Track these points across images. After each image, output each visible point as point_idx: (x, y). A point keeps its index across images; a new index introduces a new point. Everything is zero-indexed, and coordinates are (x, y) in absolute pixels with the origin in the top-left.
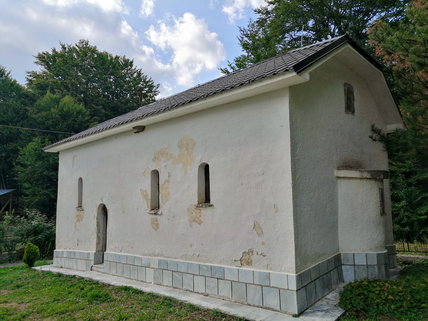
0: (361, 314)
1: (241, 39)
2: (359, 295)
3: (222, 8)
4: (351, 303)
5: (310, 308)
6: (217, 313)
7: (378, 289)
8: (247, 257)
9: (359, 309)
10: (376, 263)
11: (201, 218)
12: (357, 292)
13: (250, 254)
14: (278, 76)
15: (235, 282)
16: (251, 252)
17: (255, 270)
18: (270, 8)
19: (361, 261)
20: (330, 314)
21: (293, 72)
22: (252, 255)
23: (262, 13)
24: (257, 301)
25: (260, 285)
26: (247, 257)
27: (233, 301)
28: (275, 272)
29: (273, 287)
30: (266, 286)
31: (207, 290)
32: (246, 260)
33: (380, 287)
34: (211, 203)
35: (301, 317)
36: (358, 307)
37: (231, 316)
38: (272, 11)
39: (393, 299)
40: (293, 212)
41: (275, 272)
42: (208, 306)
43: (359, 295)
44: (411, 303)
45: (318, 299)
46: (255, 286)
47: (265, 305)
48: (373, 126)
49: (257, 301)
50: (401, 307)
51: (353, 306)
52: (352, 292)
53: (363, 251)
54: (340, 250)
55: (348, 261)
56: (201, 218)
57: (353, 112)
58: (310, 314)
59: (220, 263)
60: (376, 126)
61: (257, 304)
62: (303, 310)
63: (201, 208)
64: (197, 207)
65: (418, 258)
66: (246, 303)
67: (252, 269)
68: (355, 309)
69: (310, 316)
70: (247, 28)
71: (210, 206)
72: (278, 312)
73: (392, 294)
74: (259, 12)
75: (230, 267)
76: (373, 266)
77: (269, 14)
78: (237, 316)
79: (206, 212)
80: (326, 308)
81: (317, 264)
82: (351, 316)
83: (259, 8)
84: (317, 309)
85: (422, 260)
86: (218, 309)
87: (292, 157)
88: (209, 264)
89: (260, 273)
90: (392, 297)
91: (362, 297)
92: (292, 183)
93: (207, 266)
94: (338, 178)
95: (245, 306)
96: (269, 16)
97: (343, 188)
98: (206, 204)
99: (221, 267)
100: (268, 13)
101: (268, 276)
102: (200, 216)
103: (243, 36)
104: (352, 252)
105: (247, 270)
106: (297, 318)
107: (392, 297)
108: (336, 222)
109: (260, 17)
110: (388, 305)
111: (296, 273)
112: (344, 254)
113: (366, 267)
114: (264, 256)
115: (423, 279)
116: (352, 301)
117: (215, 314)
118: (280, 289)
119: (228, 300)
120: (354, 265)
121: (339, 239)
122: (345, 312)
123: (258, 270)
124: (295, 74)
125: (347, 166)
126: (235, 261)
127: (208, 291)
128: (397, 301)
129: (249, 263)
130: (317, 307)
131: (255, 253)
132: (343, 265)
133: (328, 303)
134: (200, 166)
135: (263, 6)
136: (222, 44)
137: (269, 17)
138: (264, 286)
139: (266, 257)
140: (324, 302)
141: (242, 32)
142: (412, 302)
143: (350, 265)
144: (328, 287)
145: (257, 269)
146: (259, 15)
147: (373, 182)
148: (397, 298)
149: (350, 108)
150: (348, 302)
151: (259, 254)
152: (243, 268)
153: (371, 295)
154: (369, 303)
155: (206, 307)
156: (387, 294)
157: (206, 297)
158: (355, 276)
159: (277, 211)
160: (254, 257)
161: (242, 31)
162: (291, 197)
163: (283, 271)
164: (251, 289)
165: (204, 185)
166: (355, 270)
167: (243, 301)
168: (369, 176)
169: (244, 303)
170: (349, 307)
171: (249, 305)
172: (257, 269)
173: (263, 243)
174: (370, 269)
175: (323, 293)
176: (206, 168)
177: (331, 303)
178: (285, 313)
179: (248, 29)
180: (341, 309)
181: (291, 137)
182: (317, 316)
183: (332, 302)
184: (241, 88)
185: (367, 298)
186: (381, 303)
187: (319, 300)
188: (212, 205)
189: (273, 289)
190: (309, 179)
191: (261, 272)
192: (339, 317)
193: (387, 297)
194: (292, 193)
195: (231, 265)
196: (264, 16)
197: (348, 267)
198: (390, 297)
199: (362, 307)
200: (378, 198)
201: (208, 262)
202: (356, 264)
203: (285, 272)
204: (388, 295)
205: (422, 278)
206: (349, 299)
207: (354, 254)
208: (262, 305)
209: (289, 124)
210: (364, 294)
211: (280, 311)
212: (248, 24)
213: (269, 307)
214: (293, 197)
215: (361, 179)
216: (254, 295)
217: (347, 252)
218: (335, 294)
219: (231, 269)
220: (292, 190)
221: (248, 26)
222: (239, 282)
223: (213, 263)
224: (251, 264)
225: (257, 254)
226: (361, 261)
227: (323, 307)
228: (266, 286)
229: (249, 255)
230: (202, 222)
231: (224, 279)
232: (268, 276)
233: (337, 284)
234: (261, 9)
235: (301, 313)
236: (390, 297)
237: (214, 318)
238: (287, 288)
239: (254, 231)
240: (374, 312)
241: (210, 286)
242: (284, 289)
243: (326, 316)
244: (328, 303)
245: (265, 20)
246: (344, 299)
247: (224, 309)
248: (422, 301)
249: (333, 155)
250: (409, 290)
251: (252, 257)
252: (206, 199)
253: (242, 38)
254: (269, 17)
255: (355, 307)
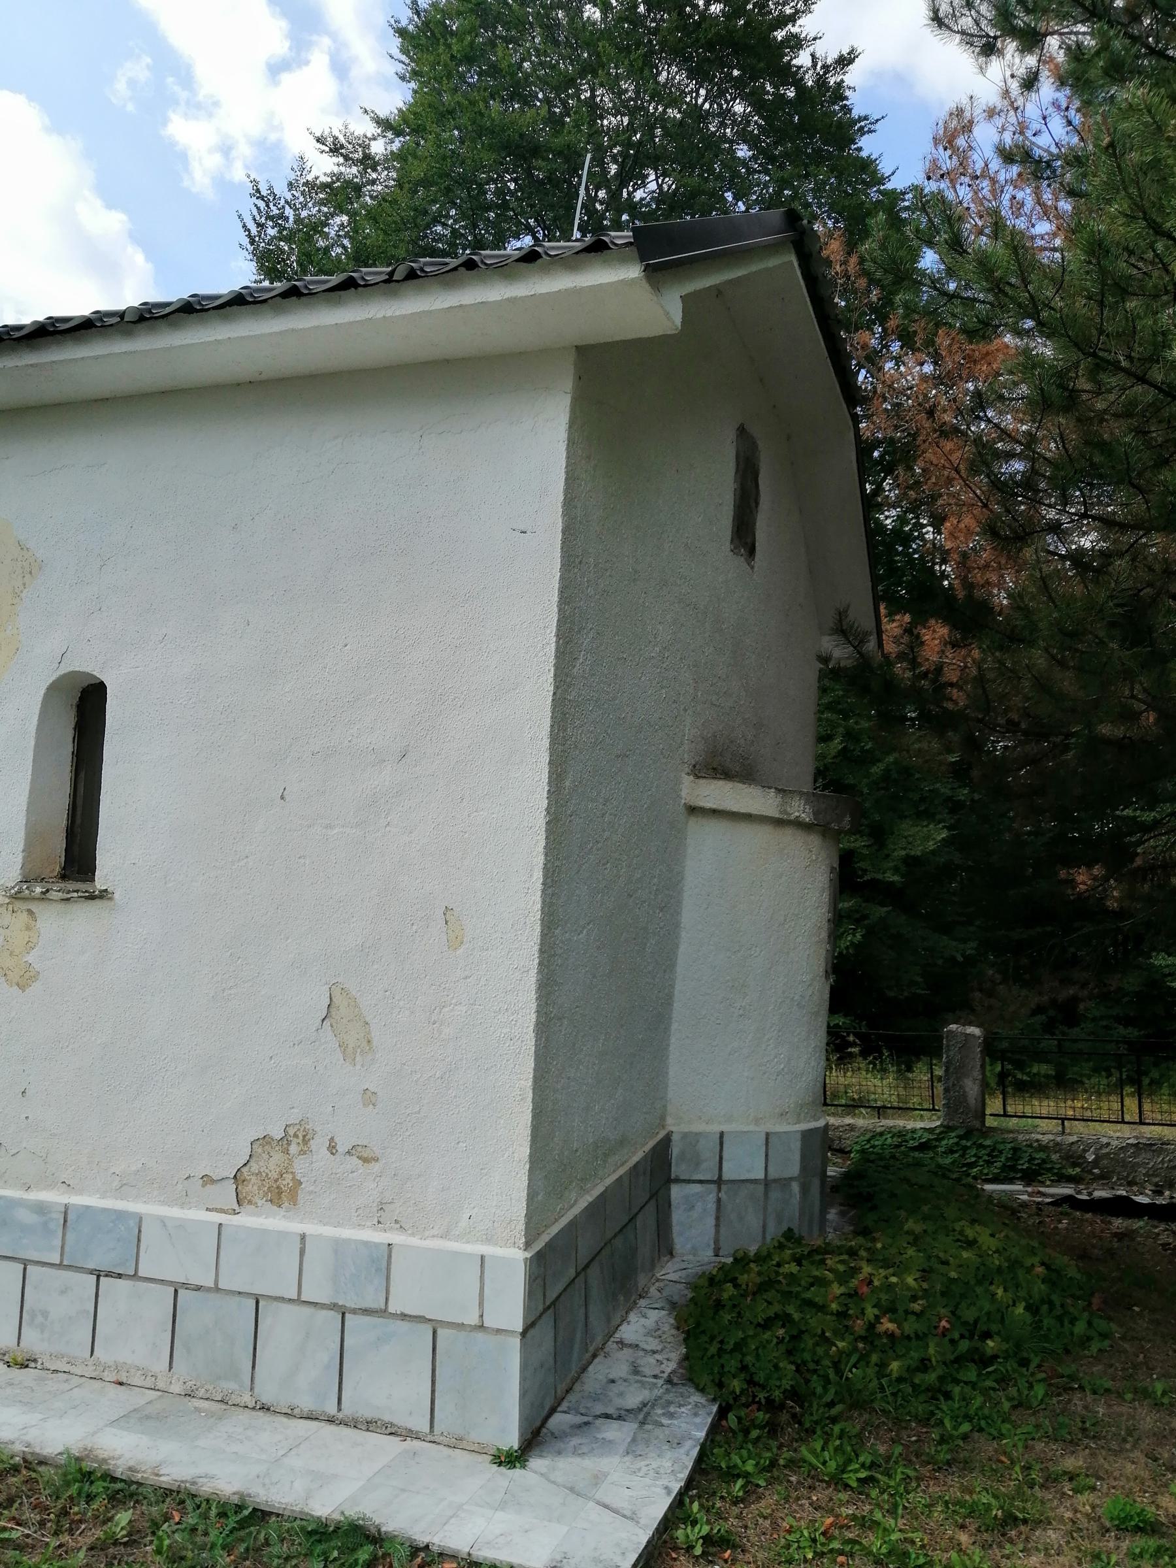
0: (784, 1417)
1: (254, 230)
2: (767, 1325)
3: (165, 122)
4: (744, 1368)
5: (564, 1406)
6: (87, 1476)
7: (837, 1289)
8: (272, 1163)
9: (777, 1394)
10: (794, 1170)
11: (30, 958)
12: (762, 1310)
13: (294, 1149)
14: (546, 270)
15: (198, 1288)
16: (297, 1137)
17: (310, 1228)
18: (378, 148)
19: (744, 1164)
20: (658, 1432)
21: (624, 261)
22: (302, 1152)
23: (346, 158)
24: (309, 1385)
25: (333, 1307)
26: (272, 1163)
27: (176, 1388)
28: (415, 1241)
29: (404, 1316)
30: (366, 1312)
31: (29, 1334)
32: (266, 1175)
33: (842, 1279)
34: (100, 883)
35: (536, 1463)
36: (774, 1382)
37: (167, 1493)
38: (386, 160)
39: (898, 1332)
40: (541, 951)
41: (415, 1241)
42: (32, 1436)
43: (767, 1325)
44: (952, 1341)
45: (591, 1349)
46: (307, 1310)
47: (348, 1409)
48: (841, 615)
49: (309, 1385)
50: (924, 1365)
51: (751, 1382)
52: (739, 1315)
53: (757, 1121)
54: (669, 1120)
55: (698, 1164)
56: (30, 958)
57: (751, 551)
58: (575, 1441)
59: (123, 1187)
60: (851, 615)
61: (306, 1403)
62: (538, 1424)
63: (34, 906)
64: (17, 897)
65: (852, 1128)
66: (247, 1399)
67: (296, 1227)
68: (762, 1396)
69: (575, 1452)
70: (282, 190)
71: (92, 897)
72: (417, 1443)
73: (890, 1310)
74: (336, 149)
75: (175, 1212)
76: (784, 1183)
77: (374, 170)
78: (206, 1488)
79: (64, 927)
80: (634, 1398)
81: (600, 1189)
82: (746, 1432)
83: (337, 134)
84: (599, 1409)
85: (863, 1134)
86: (88, 1454)
87: (557, 687)
88: (55, 1197)
89: (338, 1245)
90: (891, 1326)
91: (781, 1332)
92: (548, 810)
93: (41, 1209)
94: (693, 810)
95: (245, 1417)
96: (374, 175)
97: (708, 854)
98: (71, 885)
99: (121, 1215)
100: (368, 162)
101: (383, 1262)
102: (30, 946)
103: (263, 220)
104: (716, 1128)
105: (265, 1232)
106: (517, 1473)
107: (891, 1326)
108: (668, 1001)
109: (336, 170)
110: (874, 1358)
111: (527, 1245)
112: (685, 1136)
113: (761, 1188)
114: (366, 1160)
115: (961, 1233)
116: (749, 1359)
117: (73, 1490)
118: (436, 1327)
119: (149, 1382)
120: (719, 1182)
121: (671, 1073)
122: (722, 1413)
123: (329, 1231)
124: (633, 272)
125: (718, 764)
126: (207, 1180)
127: (33, 1341)
128: (908, 1338)
129: (282, 1194)
130: (596, 1398)
131: (319, 1145)
132: (678, 1181)
133: (636, 1371)
134: (55, 689)
135: (351, 128)
136: (150, 266)
137: (373, 182)
138: (354, 1311)
139: (376, 1167)
140: (616, 1365)
141: (262, 204)
142: (956, 1336)
143: (701, 1182)
144: (624, 1289)
145: (330, 1224)
146: (335, 160)
147: (815, 840)
148: (910, 1326)
149: (743, 536)
150: (732, 1364)
151: (341, 1149)
152: (247, 1219)
153: (815, 1322)
154: (807, 1356)
155: (18, 1447)
156: (876, 1311)
157: (16, 1373)
158: (717, 1226)
159: (455, 942)
160: (313, 1166)
161: (262, 198)
162: (538, 875)
163: (458, 1238)
164: (281, 1325)
165: (67, 789)
166: (719, 1200)
167: (231, 1386)
168: (806, 818)
169: (235, 1399)
170: (736, 1385)
171: (265, 1408)
172: (330, 1224)
173: (369, 1098)
174: (775, 1195)
175: (609, 1320)
176: (87, 706)
177: (649, 1364)
178: (456, 1443)
179: (289, 197)
180: (697, 1398)
181: (562, 591)
182: (607, 1446)
183: (651, 1360)
184: (338, 303)
185: (795, 1338)
186: (849, 1355)
187: (594, 1356)
188: (104, 895)
189: (404, 1326)
190: (607, 800)
191: (347, 1241)
192: (703, 1446)
193: (871, 1326)
194: (540, 860)
195: (183, 1201)
196: (354, 170)
197: (697, 1188)
198: (887, 1325)
199: (787, 1384)
200: (825, 909)
201: (50, 1186)
202: (726, 1177)
203: (474, 1237)
204: (877, 1317)
205: (958, 1228)
206: (739, 1347)
207: (722, 1134)
208: (332, 1409)
209: (560, 526)
210: (786, 1320)
211: (430, 1436)
212: (292, 177)
213: (369, 1414)
214: (545, 876)
215: (779, 823)
216: (294, 1357)
217: (698, 1127)
218: (654, 1315)
219: (182, 1225)
220: (543, 843)
221: (290, 184)
222: (217, 1289)
223: (80, 1192)
224: (294, 1200)
225: (332, 1149)
226: (744, 1164)
227: (621, 1394)
228: (366, 1312)
229: (286, 1152)
230: (35, 977)
231: (135, 1276)
232: (383, 1262)
233: (653, 1267)
234: (342, 139)
235: (534, 1440)
236: (887, 1325)
237: (64, 1513)
238: (473, 1320)
239: (327, 1033)
240: (829, 1398)
241: (45, 1314)
242: (460, 1326)
243: (647, 1442)
244: (636, 1371)
245: (358, 189)
246: (713, 1350)
247: (127, 1449)
248: (982, 1327)
249: (685, 710)
250: (938, 1287)
251: (300, 1166)
252: (73, 857)
253: (259, 225)
254: (373, 182)
255: (763, 1387)
